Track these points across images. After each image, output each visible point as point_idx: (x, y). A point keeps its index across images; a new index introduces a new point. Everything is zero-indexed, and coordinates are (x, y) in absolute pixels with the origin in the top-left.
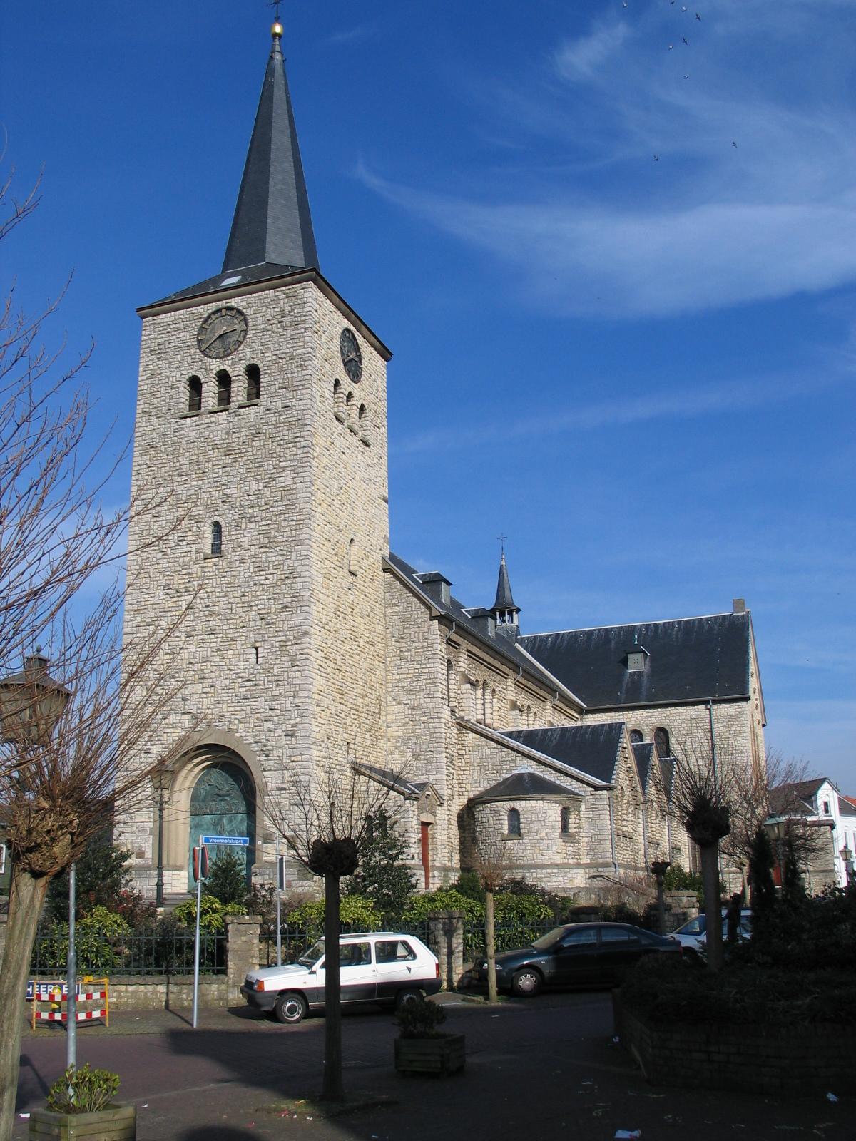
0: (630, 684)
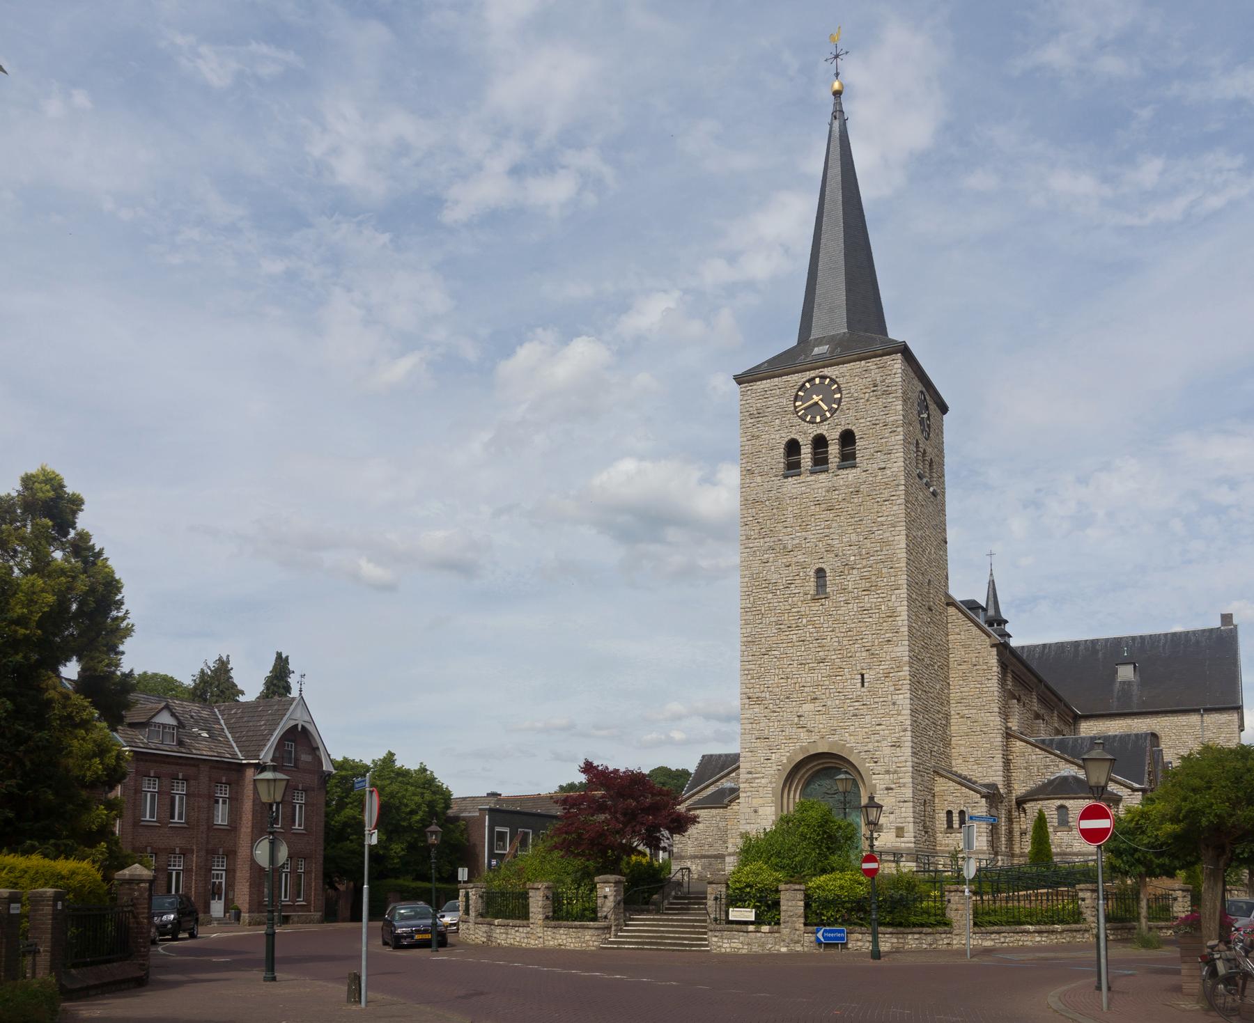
0: (1120, 693)
